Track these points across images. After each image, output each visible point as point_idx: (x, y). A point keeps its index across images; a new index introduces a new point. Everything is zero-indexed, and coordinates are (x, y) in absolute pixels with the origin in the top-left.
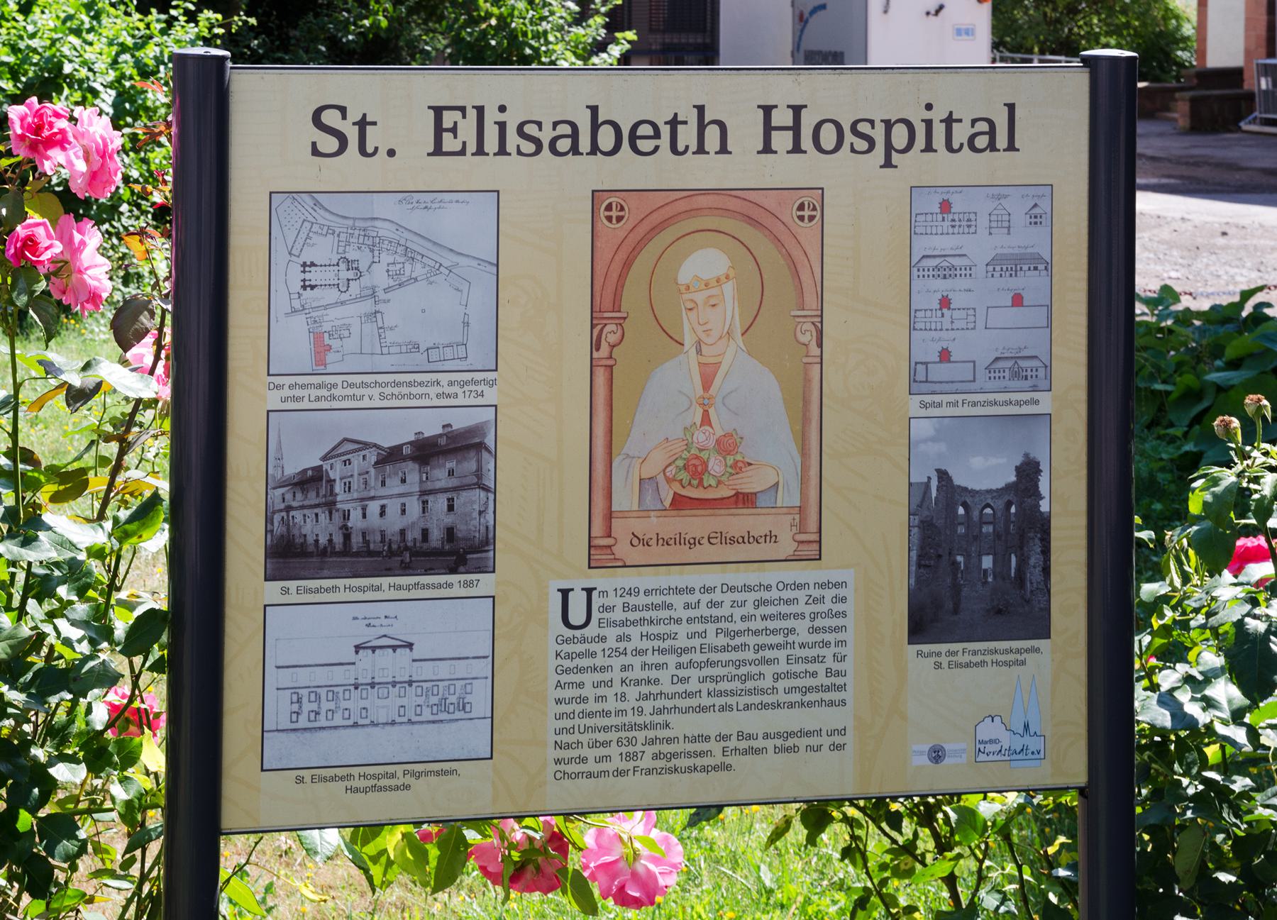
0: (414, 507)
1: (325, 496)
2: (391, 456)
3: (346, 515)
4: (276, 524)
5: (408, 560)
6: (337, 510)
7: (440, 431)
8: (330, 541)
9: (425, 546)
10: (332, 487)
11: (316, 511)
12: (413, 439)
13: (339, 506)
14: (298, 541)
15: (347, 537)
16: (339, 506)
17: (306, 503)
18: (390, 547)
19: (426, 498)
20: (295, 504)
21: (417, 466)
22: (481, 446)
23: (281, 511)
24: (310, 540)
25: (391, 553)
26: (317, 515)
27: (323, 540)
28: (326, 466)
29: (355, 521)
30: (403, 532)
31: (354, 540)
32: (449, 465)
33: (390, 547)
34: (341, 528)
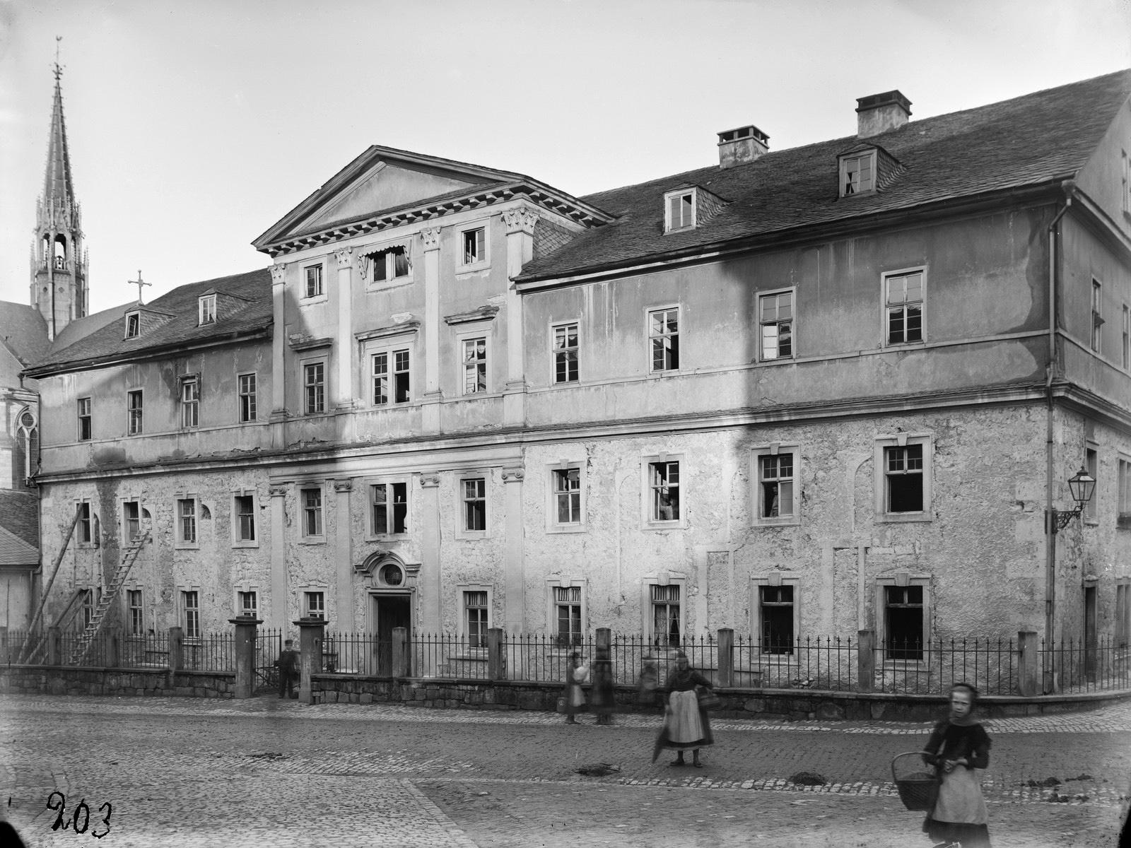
0: (718, 474)
1: (284, 417)
2: (608, 239)
3: (390, 512)
4: (51, 538)
5: (692, 732)
6: (345, 486)
7: (848, 126)
8: (313, 626)
9: (779, 669)
10: (316, 374)
11: (242, 482)
12: (709, 156)
13: (351, 466)
14: (162, 618)
15: (394, 612)
16: (351, 466)
17: (193, 445)
18: (603, 663)
19: (776, 441)
20: (139, 450)
21: (734, 290)
22: (1053, 204)
23: (74, 477)
24: (217, 617)
25: (607, 698)
26: (246, 502)
27: (279, 622)
28: (289, 277)
29: (434, 542)
30: (665, 598)
31: (425, 620)
32: (896, 291)
33: (603, 663)
34: (363, 570)
